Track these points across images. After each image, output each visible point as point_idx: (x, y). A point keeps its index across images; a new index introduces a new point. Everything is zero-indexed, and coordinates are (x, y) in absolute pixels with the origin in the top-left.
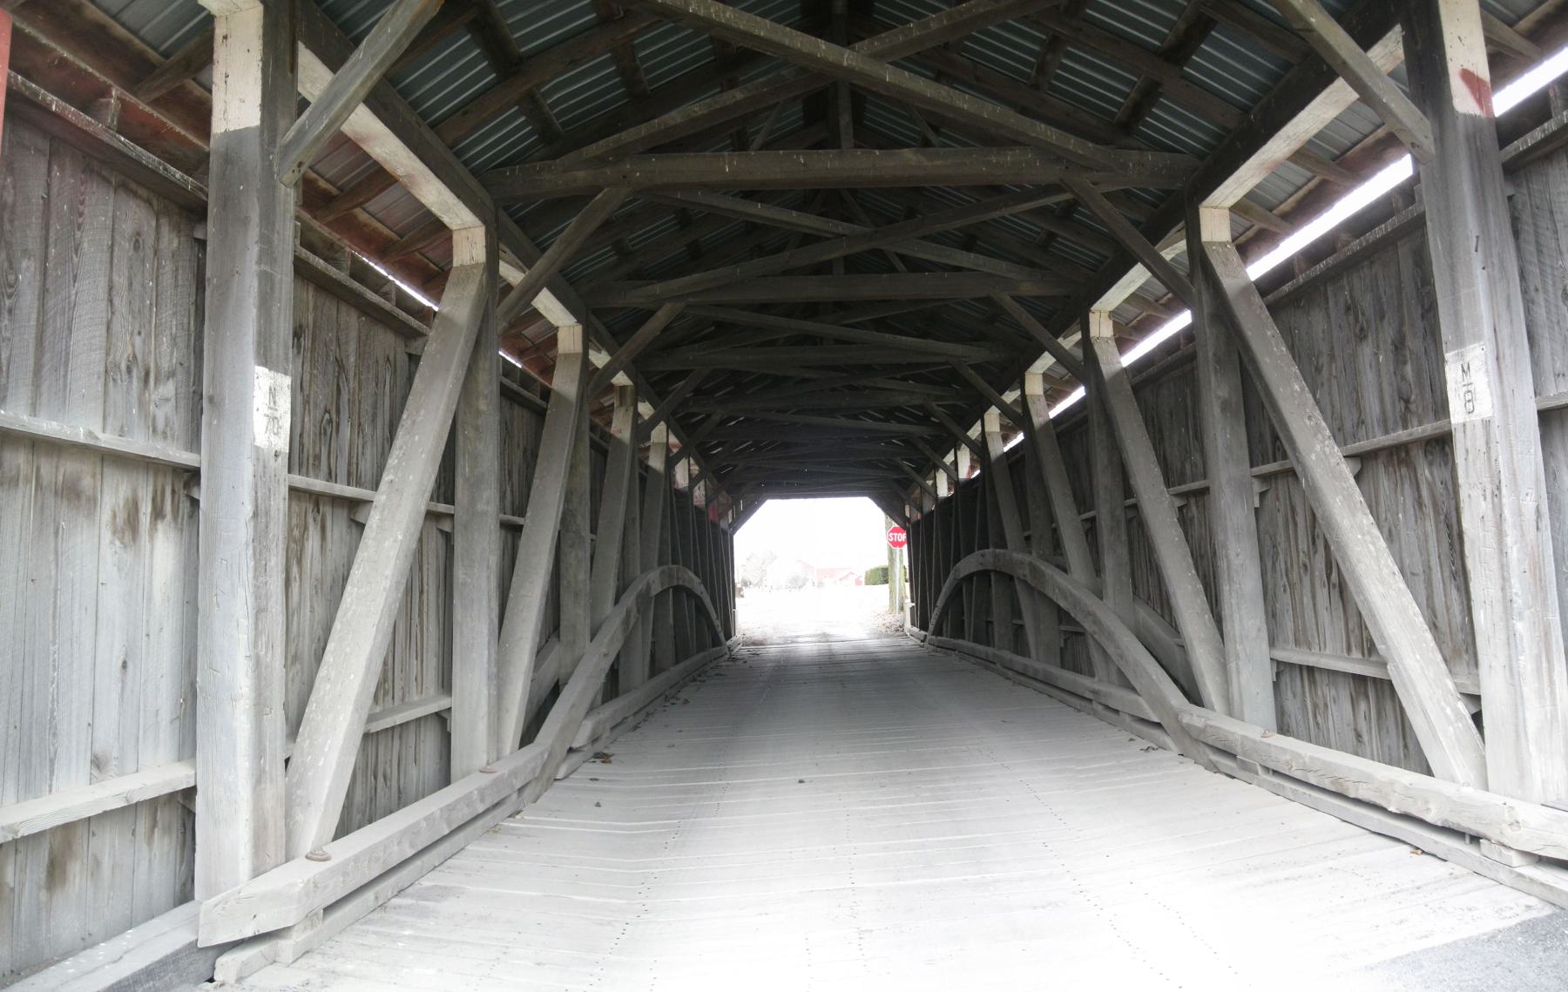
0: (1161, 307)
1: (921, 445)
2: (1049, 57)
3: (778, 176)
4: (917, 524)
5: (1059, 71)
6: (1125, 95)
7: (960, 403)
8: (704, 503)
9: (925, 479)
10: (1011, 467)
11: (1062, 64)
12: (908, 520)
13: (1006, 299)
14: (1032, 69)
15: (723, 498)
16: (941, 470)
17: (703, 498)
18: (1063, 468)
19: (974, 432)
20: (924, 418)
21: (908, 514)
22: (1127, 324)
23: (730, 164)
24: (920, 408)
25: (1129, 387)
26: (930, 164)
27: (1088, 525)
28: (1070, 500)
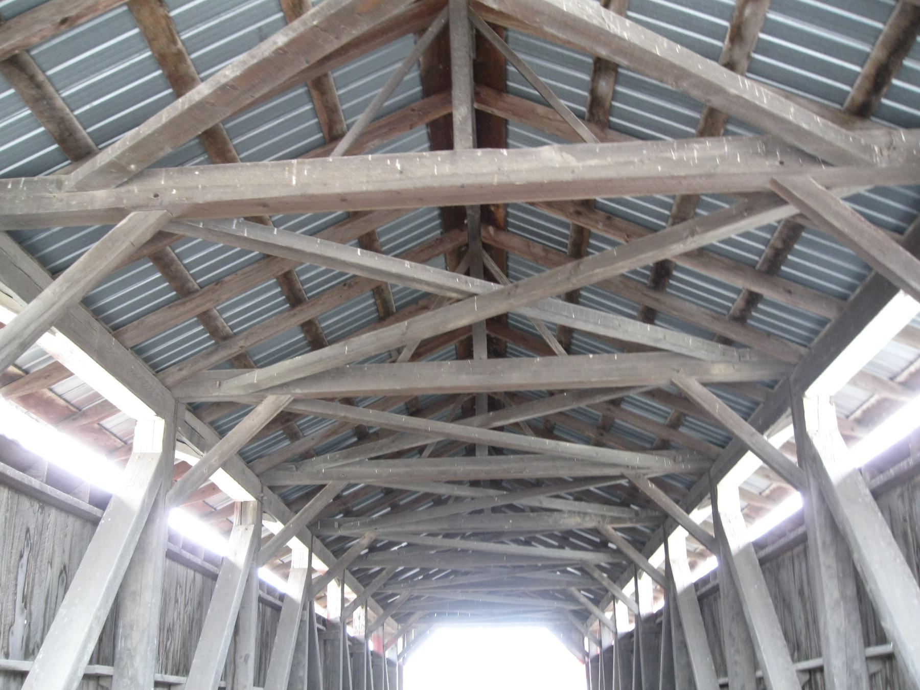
0: (899, 388)
1: (597, 574)
2: (748, 11)
3: (364, 188)
4: (595, 659)
5: (763, 36)
6: (858, 57)
7: (639, 526)
8: (363, 634)
9: (603, 611)
10: (701, 599)
11: (767, 20)
12: (587, 654)
13: (694, 387)
14: (723, 41)
15: (391, 626)
16: (620, 602)
17: (363, 629)
18: (770, 601)
19: (657, 560)
20: (602, 545)
21: (587, 649)
22: (847, 417)
23: (299, 174)
24: (595, 531)
25: (868, 492)
26: (580, 164)
27: (806, 677)
28: (781, 642)
